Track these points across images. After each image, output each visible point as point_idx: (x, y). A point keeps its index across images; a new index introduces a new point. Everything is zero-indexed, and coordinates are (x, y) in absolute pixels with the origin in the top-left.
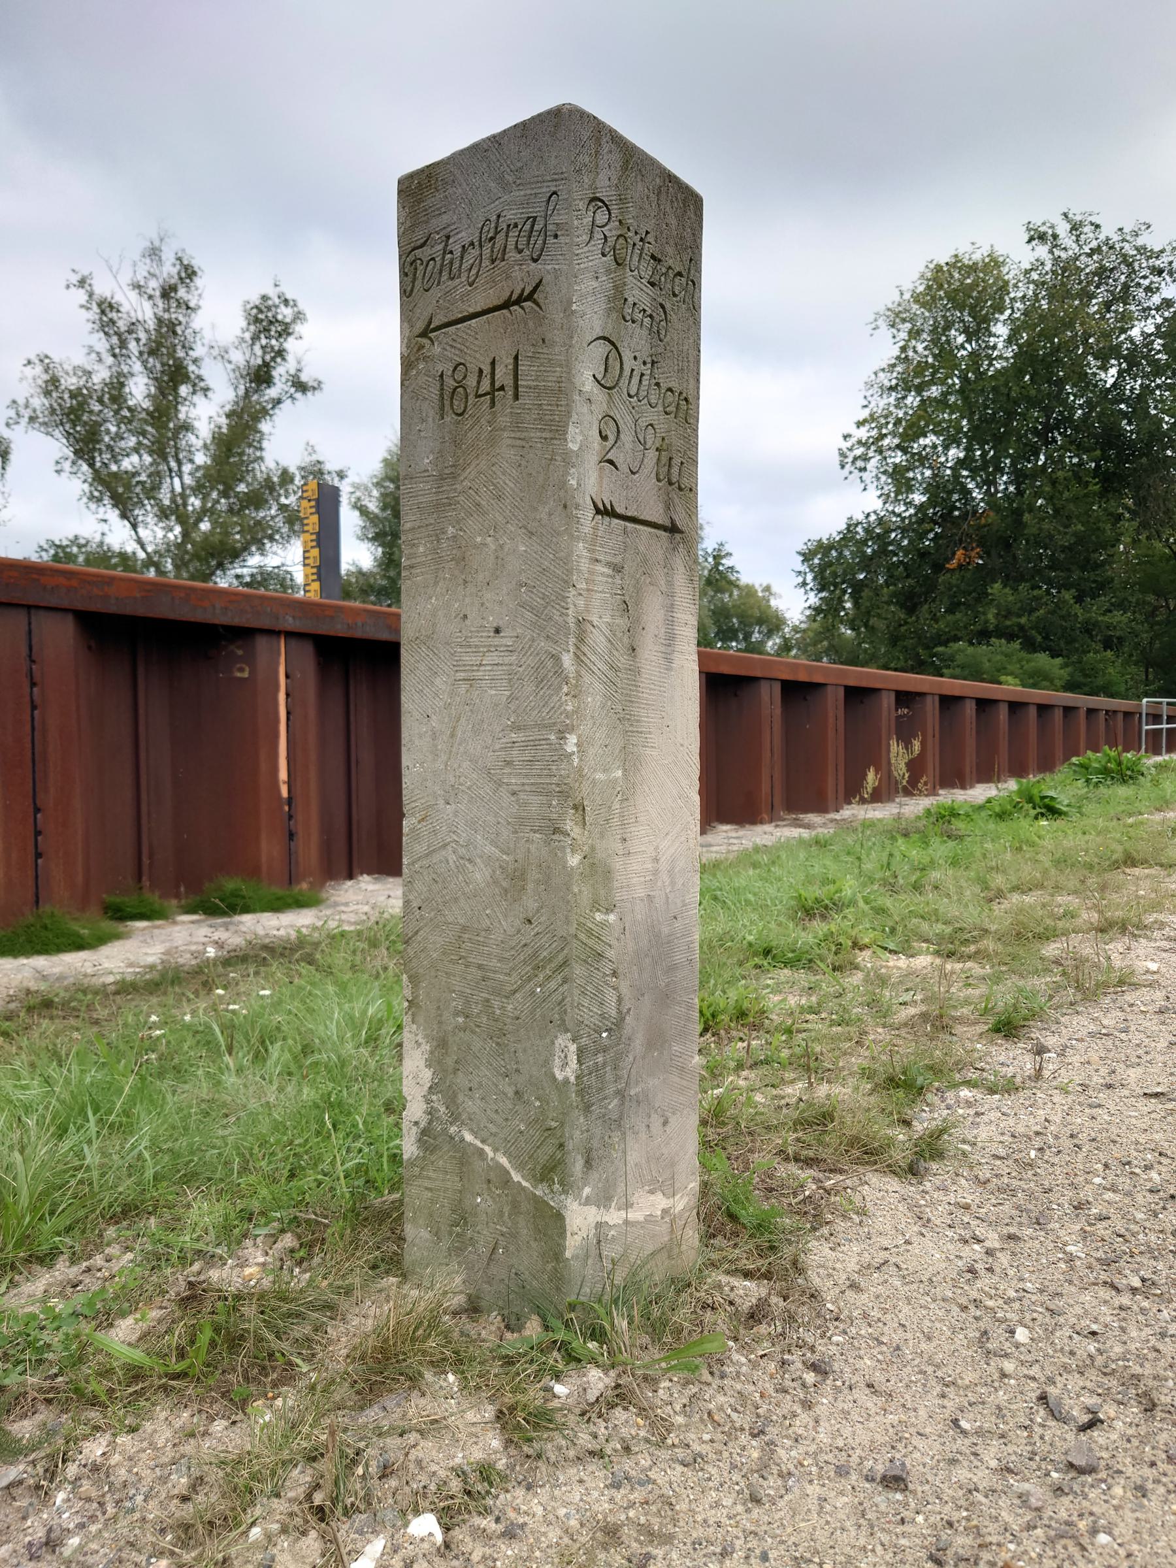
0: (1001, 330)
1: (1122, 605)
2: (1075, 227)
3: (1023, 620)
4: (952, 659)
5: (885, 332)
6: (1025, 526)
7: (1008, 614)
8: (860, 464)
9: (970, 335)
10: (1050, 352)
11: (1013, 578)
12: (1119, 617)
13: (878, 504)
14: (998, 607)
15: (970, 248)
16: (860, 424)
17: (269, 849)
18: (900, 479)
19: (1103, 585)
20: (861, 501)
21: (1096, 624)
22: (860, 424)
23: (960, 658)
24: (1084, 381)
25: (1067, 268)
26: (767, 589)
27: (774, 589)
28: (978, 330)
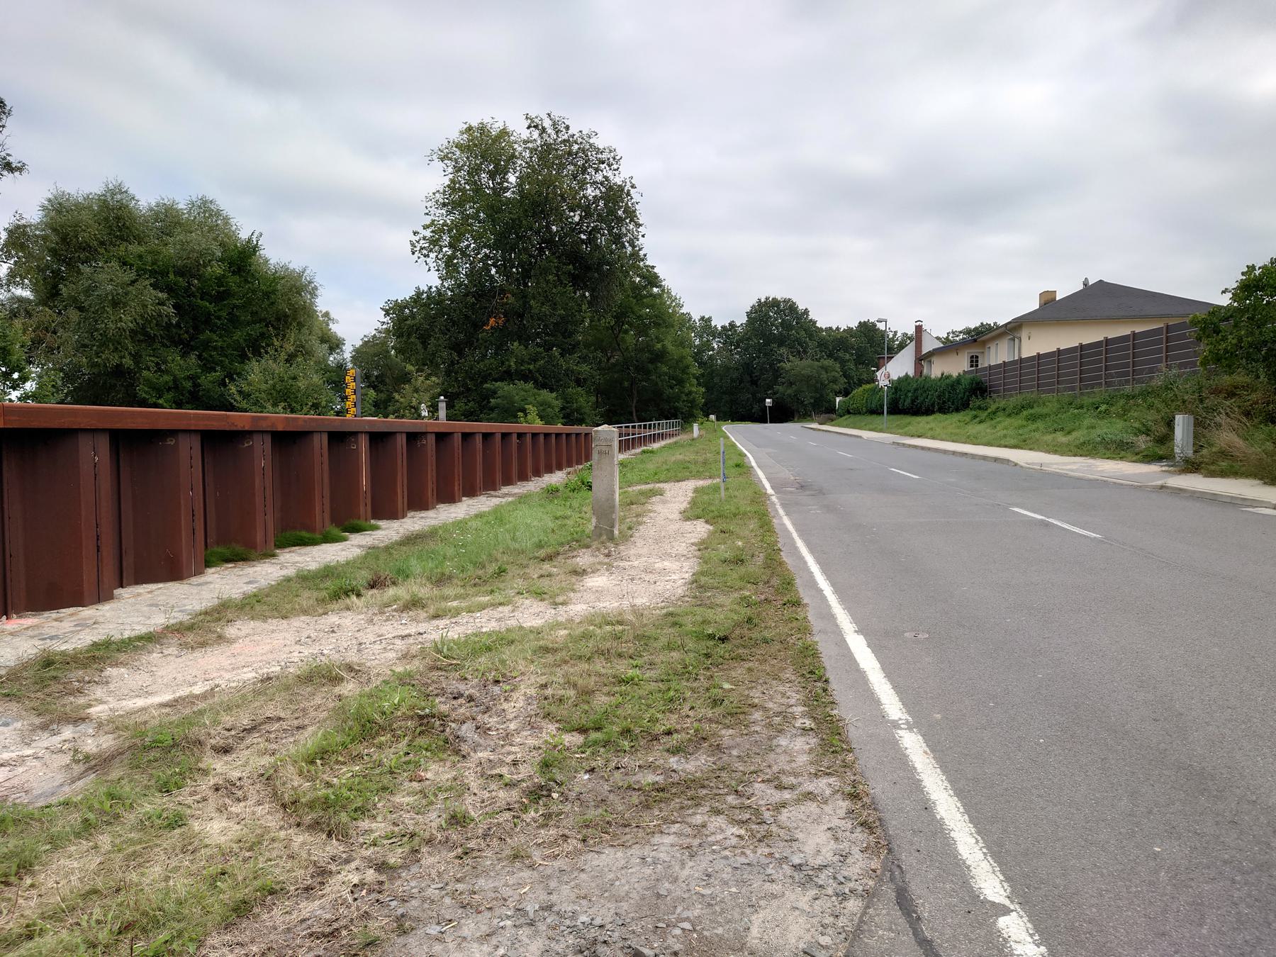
0: (512, 178)
1: (584, 359)
2: (554, 124)
3: (531, 367)
4: (495, 392)
5: (668, 494)
6: (531, 307)
7: (523, 362)
8: (425, 252)
9: (492, 175)
10: (539, 203)
11: (524, 338)
12: (585, 368)
13: (438, 282)
14: (516, 357)
15: (491, 121)
16: (425, 227)
17: (259, 537)
18: (450, 266)
19: (575, 346)
20: (426, 277)
21: (572, 371)
22: (425, 227)
23: (500, 393)
24: (561, 217)
25: (547, 149)
26: (327, 314)
27: (332, 315)
28: (499, 172)
